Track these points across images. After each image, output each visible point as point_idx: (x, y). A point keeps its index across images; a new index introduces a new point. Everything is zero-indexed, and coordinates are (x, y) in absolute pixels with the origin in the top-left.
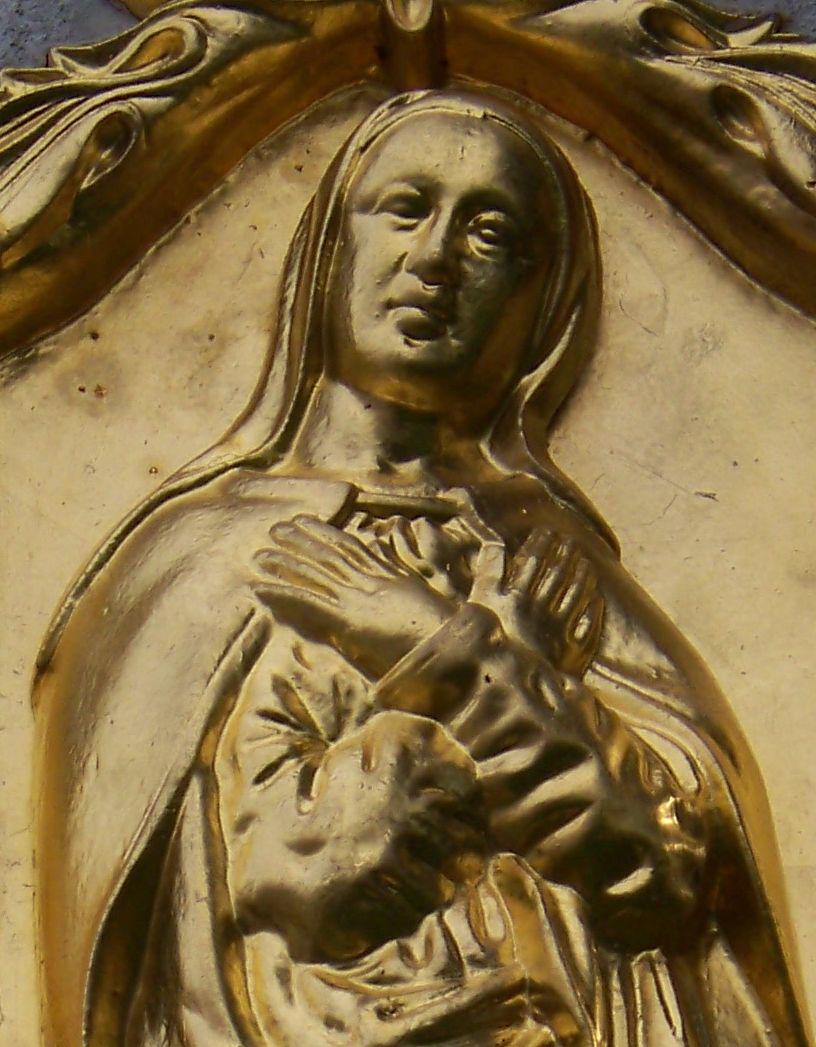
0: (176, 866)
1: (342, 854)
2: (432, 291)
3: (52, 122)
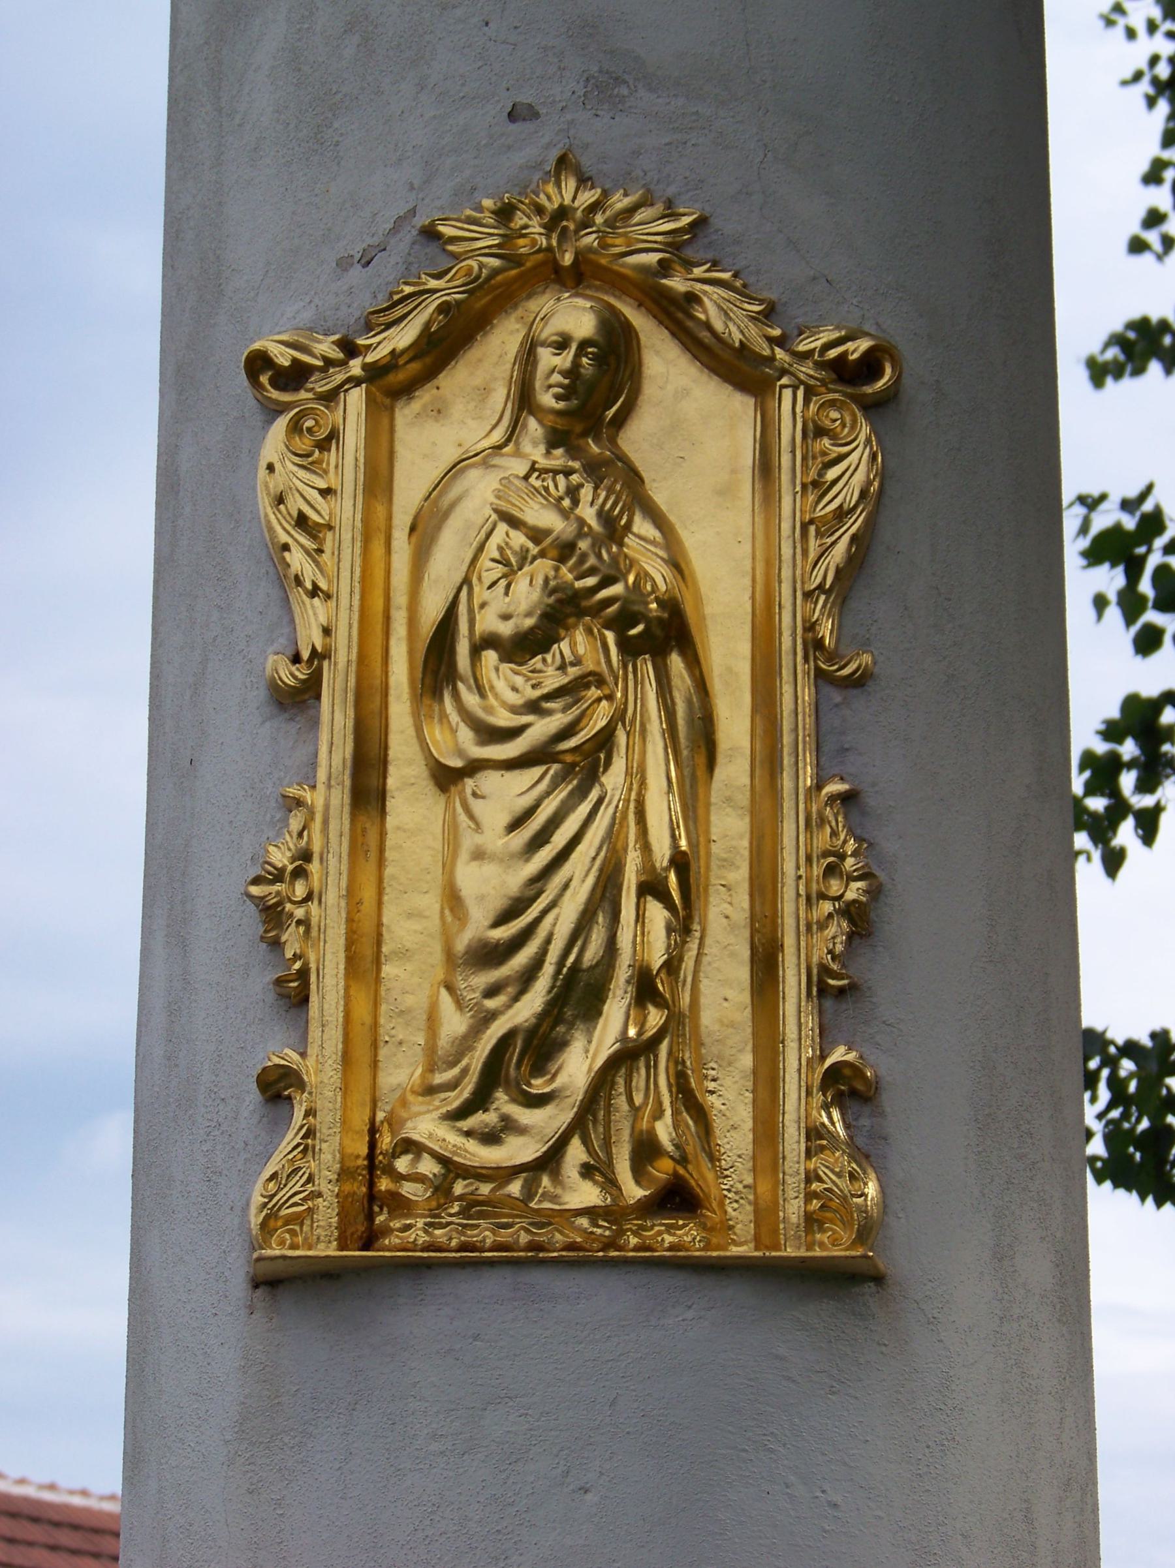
0: (456, 623)
1: (519, 622)
2: (567, 381)
3: (420, 304)
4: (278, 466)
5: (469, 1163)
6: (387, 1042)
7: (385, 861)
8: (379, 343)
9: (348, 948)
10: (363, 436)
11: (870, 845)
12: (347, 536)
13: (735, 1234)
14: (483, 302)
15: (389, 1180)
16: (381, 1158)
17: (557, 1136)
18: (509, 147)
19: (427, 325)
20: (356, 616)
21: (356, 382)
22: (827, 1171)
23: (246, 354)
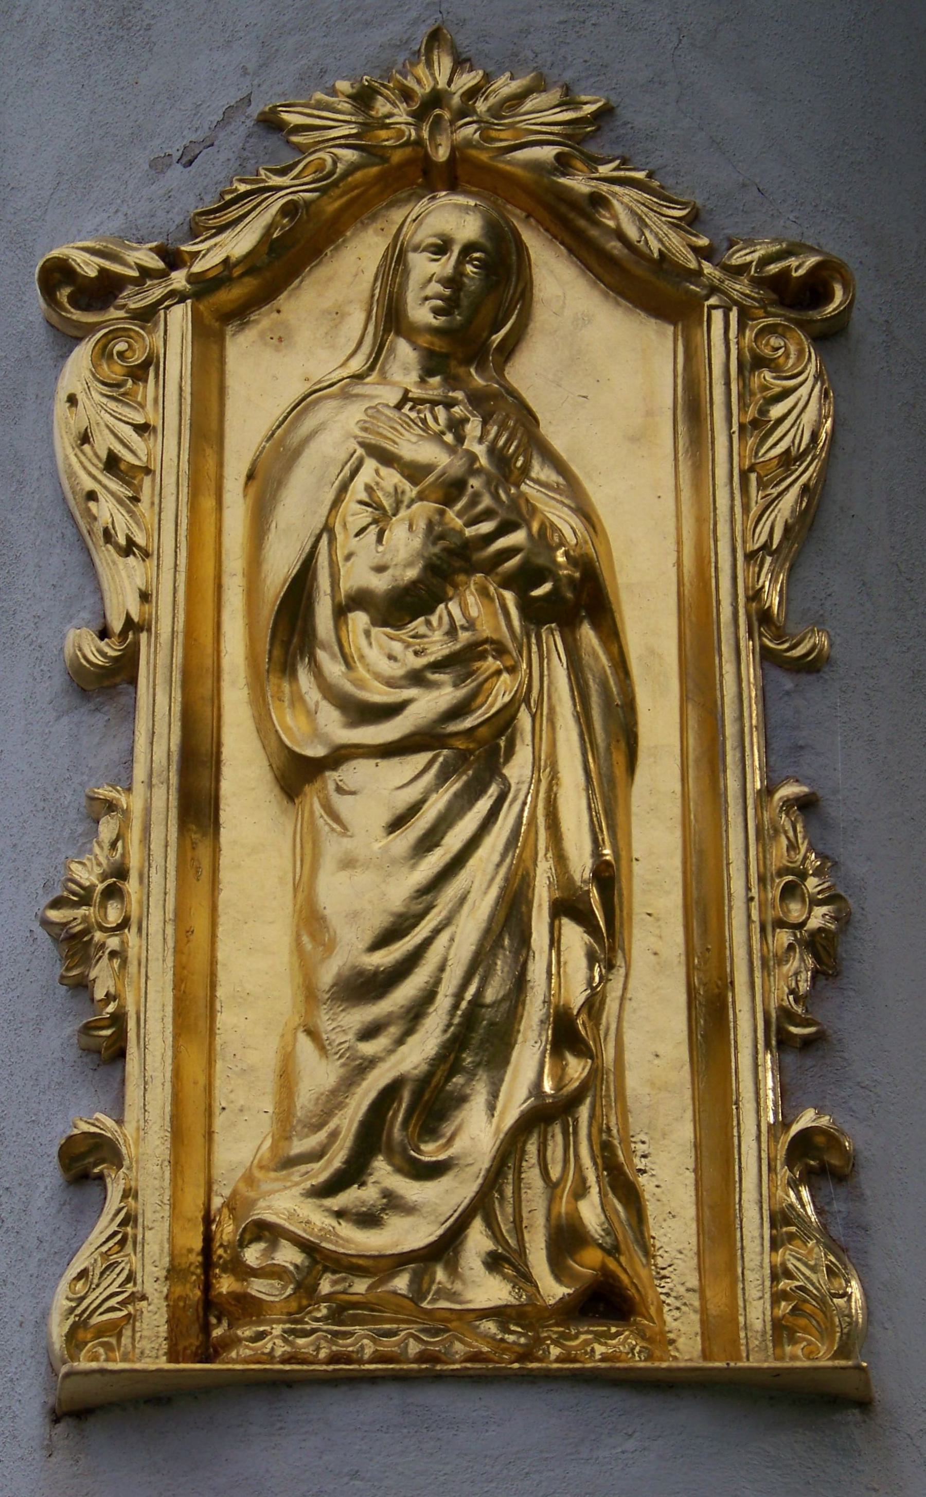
0: (314, 578)
2: (448, 292)
4: (81, 397)
5: (342, 1250)
6: (224, 1109)
7: (219, 883)
8: (208, 250)
9: (176, 987)
10: (189, 360)
11: (835, 864)
12: (169, 481)
13: (677, 1350)
14: (337, 204)
15: (232, 1279)
16: (220, 1251)
17: (456, 1215)
18: (367, 24)
19: (270, 228)
20: (182, 578)
21: (179, 297)
22: (798, 1264)
23: (41, 263)
